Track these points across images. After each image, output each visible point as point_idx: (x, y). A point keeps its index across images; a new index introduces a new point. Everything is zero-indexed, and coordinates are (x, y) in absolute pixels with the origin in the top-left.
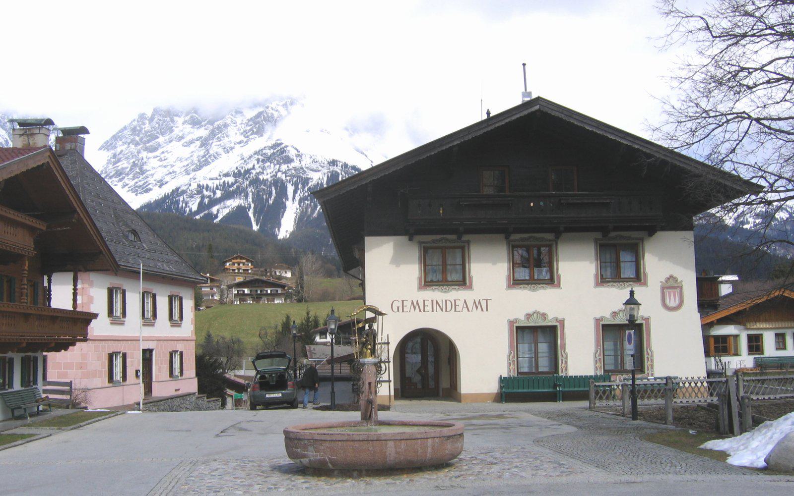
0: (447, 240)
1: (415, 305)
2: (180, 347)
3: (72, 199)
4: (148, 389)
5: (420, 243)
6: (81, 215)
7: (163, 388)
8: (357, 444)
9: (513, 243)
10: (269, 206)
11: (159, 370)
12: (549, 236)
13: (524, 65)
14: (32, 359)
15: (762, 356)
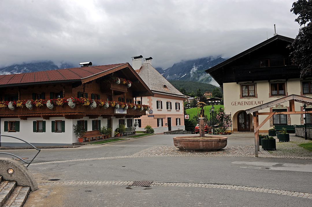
0: (249, 83)
1: (239, 103)
2: (179, 117)
4: (170, 129)
5: (240, 84)
6: (140, 81)
8: (191, 142)
9: (271, 83)
11: (173, 122)
12: (285, 80)
13: (275, 25)
15: (79, 120)
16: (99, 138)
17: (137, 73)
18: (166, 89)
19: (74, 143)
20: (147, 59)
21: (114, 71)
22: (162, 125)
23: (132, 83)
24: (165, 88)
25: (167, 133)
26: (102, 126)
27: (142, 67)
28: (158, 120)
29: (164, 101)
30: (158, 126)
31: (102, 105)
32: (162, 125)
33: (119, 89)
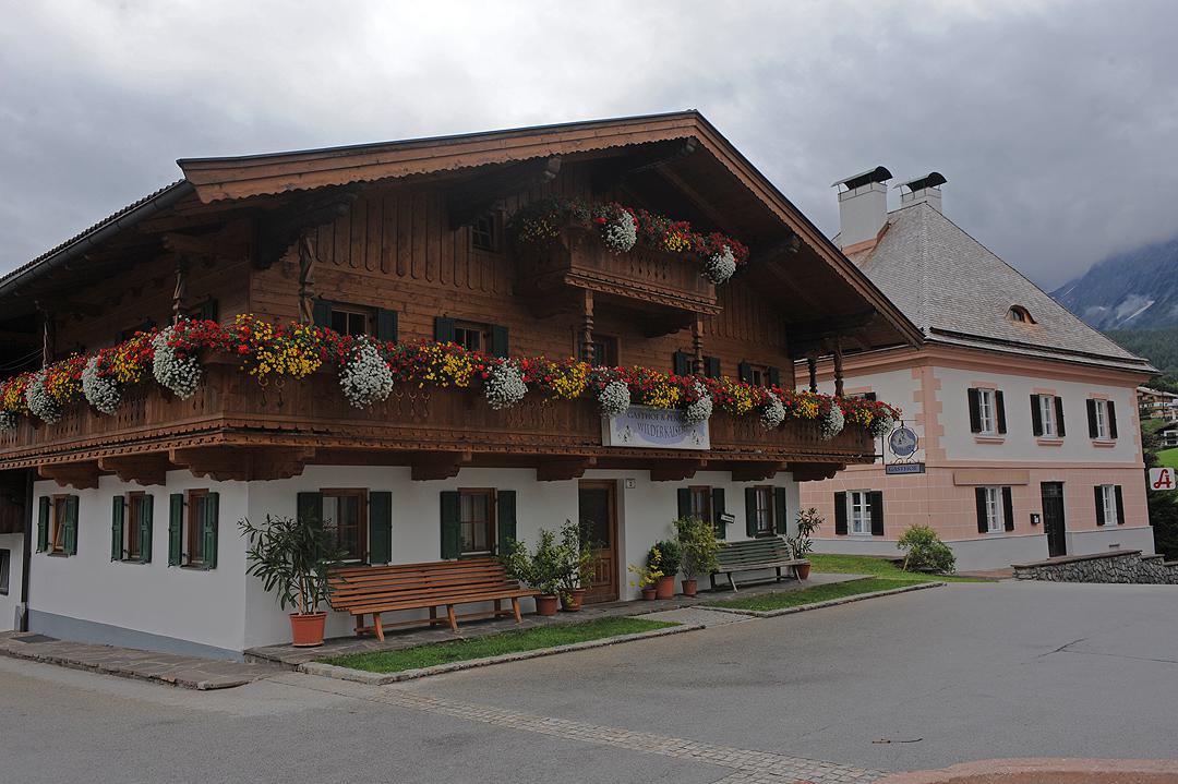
2: (1109, 479)
3: (774, 208)
4: (1057, 543)
6: (806, 239)
7: (1084, 539)
10: (563, 278)
14: (774, 492)
16: (779, 573)
18: (1026, 326)
19: (258, 644)
20: (915, 186)
21: (558, 149)
22: (1009, 526)
23: (745, 251)
24: (1022, 319)
25: (1035, 571)
26: (528, 538)
27: (888, 226)
28: (981, 494)
29: (1017, 392)
30: (983, 527)
31: (450, 379)
32: (1009, 526)
33: (648, 285)
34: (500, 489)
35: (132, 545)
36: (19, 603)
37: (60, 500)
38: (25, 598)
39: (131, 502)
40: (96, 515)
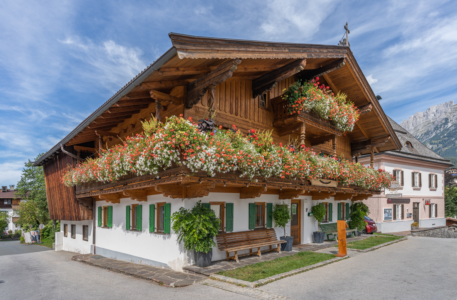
7: (425, 222)
17: (396, 132)
22: (403, 217)
34: (227, 202)
35: (134, 225)
36: (92, 244)
37: (105, 208)
38: (94, 242)
39: (133, 208)
40: (120, 211)
